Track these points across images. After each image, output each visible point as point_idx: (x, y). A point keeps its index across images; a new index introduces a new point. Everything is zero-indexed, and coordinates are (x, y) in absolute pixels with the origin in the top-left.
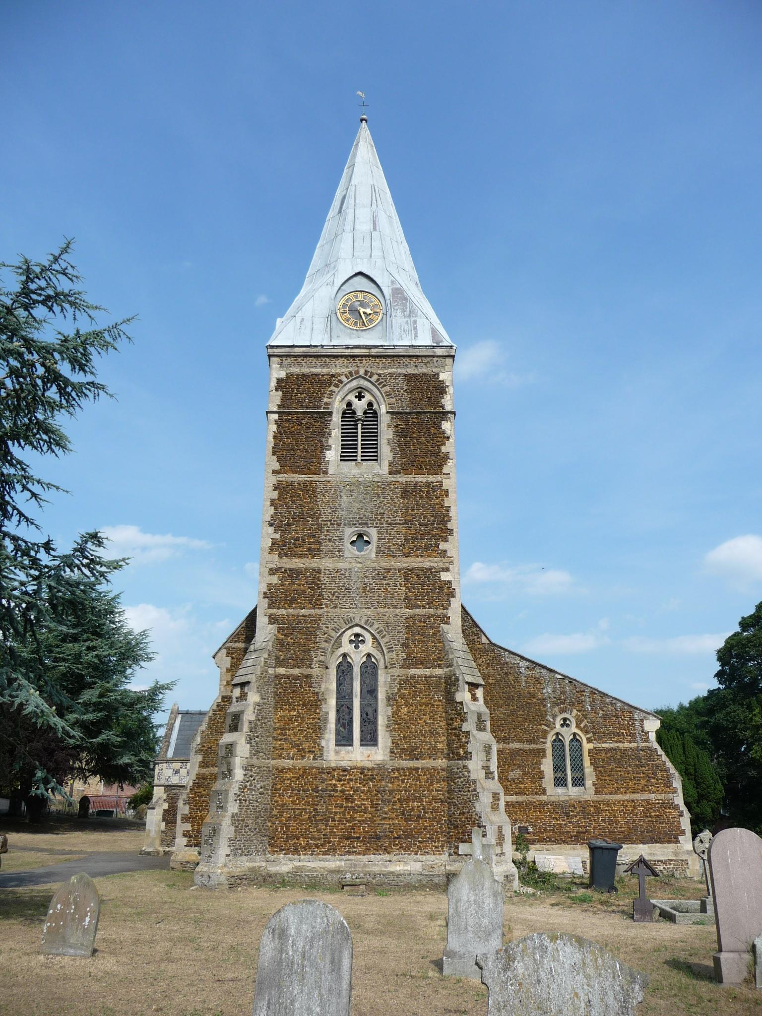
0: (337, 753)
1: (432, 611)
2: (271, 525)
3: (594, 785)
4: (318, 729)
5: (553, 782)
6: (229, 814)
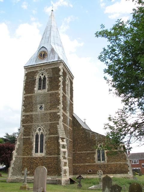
0: (35, 154)
1: (55, 122)
2: (23, 106)
3: (107, 160)
4: (32, 149)
5: (97, 160)
6: (11, 167)
